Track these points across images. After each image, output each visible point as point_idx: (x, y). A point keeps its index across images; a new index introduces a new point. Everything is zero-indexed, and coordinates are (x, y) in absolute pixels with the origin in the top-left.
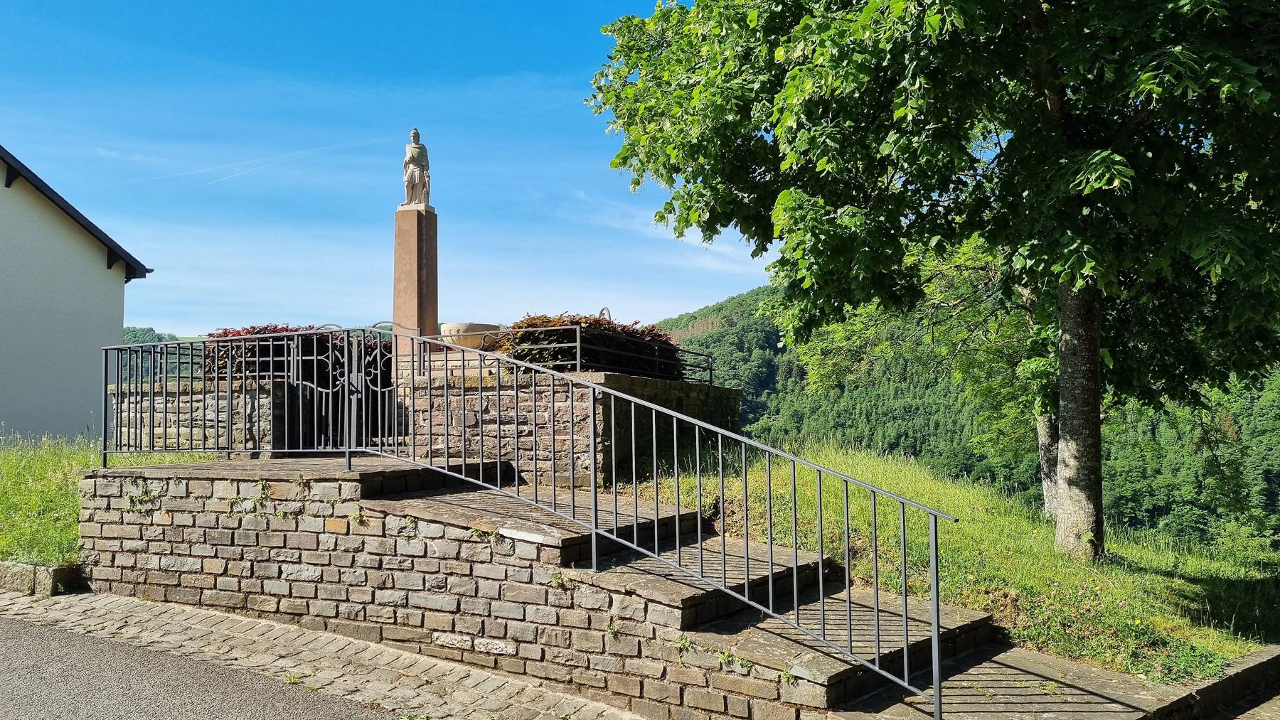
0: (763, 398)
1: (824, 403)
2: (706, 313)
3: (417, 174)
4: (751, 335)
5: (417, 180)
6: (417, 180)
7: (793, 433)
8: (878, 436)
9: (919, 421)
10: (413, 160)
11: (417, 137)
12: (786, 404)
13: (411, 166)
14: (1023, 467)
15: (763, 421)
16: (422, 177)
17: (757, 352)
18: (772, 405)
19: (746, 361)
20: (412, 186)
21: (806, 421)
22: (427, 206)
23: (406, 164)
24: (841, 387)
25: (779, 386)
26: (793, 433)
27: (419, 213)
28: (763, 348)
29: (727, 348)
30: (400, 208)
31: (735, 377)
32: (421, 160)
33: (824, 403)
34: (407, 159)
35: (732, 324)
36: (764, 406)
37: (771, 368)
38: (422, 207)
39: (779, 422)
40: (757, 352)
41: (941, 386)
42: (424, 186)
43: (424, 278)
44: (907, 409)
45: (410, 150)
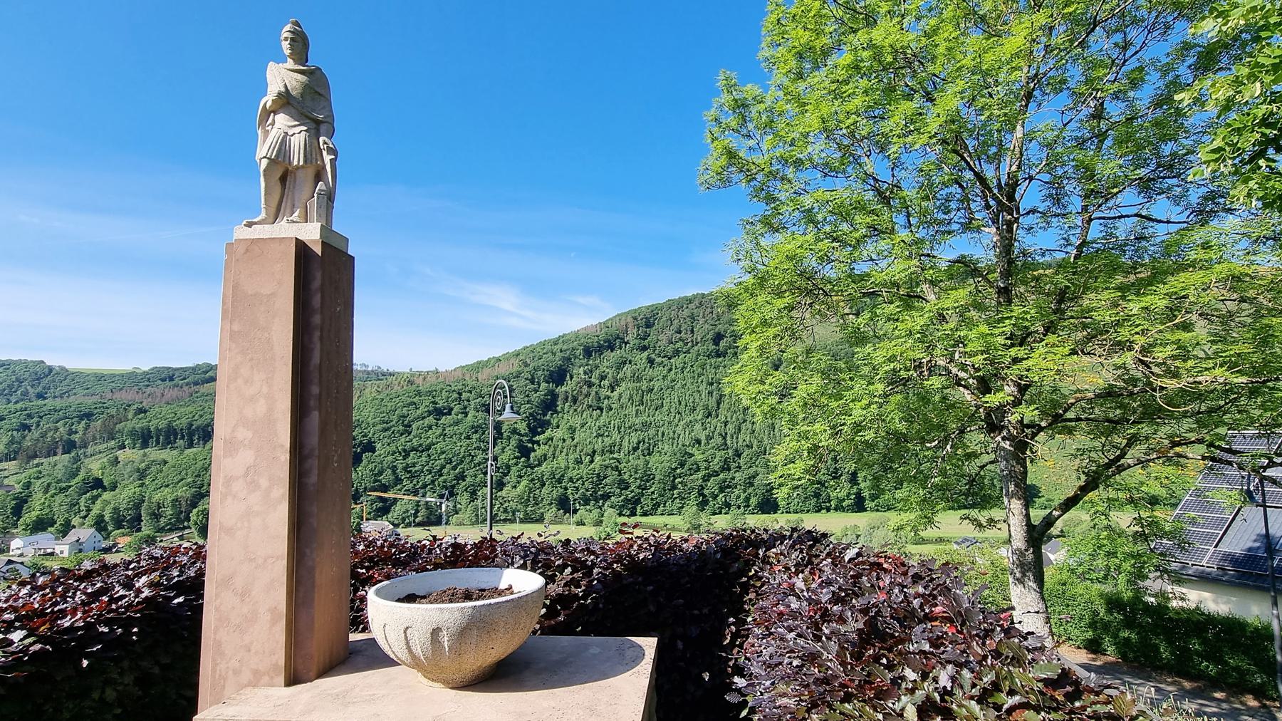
0: (548, 417)
1: (589, 420)
2: (508, 357)
3: (298, 140)
4: (540, 373)
5: (297, 159)
6: (297, 159)
7: (569, 442)
8: (625, 443)
9: (652, 432)
10: (286, 102)
11: (300, 44)
12: (564, 422)
13: (282, 121)
14: (716, 461)
15: (548, 433)
16: (312, 151)
17: (543, 385)
18: (554, 422)
19: (536, 391)
20: (282, 174)
21: (577, 433)
22: (326, 230)
23: (267, 113)
24: (601, 409)
25: (559, 409)
26: (569, 442)
27: (302, 249)
28: (548, 382)
29: (523, 382)
30: (242, 233)
31: (529, 402)
32: (310, 104)
33: (589, 420)
34: (268, 100)
35: (526, 365)
36: (549, 423)
37: (554, 396)
38: (311, 233)
39: (559, 434)
40: (543, 385)
41: (665, 408)
42: (319, 176)
43: (313, 440)
44: (644, 424)
45: (281, 76)
